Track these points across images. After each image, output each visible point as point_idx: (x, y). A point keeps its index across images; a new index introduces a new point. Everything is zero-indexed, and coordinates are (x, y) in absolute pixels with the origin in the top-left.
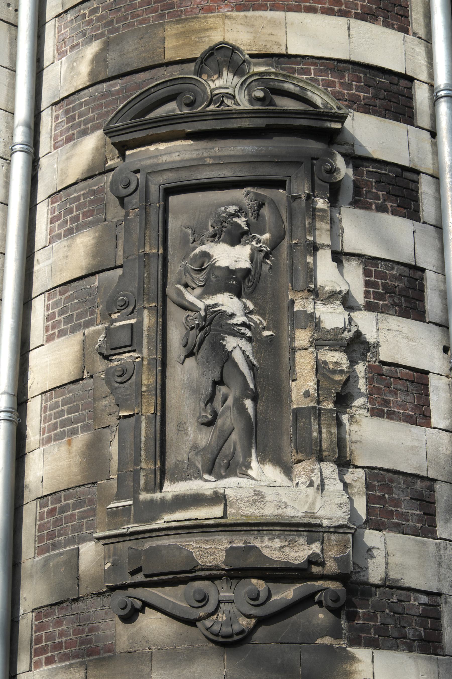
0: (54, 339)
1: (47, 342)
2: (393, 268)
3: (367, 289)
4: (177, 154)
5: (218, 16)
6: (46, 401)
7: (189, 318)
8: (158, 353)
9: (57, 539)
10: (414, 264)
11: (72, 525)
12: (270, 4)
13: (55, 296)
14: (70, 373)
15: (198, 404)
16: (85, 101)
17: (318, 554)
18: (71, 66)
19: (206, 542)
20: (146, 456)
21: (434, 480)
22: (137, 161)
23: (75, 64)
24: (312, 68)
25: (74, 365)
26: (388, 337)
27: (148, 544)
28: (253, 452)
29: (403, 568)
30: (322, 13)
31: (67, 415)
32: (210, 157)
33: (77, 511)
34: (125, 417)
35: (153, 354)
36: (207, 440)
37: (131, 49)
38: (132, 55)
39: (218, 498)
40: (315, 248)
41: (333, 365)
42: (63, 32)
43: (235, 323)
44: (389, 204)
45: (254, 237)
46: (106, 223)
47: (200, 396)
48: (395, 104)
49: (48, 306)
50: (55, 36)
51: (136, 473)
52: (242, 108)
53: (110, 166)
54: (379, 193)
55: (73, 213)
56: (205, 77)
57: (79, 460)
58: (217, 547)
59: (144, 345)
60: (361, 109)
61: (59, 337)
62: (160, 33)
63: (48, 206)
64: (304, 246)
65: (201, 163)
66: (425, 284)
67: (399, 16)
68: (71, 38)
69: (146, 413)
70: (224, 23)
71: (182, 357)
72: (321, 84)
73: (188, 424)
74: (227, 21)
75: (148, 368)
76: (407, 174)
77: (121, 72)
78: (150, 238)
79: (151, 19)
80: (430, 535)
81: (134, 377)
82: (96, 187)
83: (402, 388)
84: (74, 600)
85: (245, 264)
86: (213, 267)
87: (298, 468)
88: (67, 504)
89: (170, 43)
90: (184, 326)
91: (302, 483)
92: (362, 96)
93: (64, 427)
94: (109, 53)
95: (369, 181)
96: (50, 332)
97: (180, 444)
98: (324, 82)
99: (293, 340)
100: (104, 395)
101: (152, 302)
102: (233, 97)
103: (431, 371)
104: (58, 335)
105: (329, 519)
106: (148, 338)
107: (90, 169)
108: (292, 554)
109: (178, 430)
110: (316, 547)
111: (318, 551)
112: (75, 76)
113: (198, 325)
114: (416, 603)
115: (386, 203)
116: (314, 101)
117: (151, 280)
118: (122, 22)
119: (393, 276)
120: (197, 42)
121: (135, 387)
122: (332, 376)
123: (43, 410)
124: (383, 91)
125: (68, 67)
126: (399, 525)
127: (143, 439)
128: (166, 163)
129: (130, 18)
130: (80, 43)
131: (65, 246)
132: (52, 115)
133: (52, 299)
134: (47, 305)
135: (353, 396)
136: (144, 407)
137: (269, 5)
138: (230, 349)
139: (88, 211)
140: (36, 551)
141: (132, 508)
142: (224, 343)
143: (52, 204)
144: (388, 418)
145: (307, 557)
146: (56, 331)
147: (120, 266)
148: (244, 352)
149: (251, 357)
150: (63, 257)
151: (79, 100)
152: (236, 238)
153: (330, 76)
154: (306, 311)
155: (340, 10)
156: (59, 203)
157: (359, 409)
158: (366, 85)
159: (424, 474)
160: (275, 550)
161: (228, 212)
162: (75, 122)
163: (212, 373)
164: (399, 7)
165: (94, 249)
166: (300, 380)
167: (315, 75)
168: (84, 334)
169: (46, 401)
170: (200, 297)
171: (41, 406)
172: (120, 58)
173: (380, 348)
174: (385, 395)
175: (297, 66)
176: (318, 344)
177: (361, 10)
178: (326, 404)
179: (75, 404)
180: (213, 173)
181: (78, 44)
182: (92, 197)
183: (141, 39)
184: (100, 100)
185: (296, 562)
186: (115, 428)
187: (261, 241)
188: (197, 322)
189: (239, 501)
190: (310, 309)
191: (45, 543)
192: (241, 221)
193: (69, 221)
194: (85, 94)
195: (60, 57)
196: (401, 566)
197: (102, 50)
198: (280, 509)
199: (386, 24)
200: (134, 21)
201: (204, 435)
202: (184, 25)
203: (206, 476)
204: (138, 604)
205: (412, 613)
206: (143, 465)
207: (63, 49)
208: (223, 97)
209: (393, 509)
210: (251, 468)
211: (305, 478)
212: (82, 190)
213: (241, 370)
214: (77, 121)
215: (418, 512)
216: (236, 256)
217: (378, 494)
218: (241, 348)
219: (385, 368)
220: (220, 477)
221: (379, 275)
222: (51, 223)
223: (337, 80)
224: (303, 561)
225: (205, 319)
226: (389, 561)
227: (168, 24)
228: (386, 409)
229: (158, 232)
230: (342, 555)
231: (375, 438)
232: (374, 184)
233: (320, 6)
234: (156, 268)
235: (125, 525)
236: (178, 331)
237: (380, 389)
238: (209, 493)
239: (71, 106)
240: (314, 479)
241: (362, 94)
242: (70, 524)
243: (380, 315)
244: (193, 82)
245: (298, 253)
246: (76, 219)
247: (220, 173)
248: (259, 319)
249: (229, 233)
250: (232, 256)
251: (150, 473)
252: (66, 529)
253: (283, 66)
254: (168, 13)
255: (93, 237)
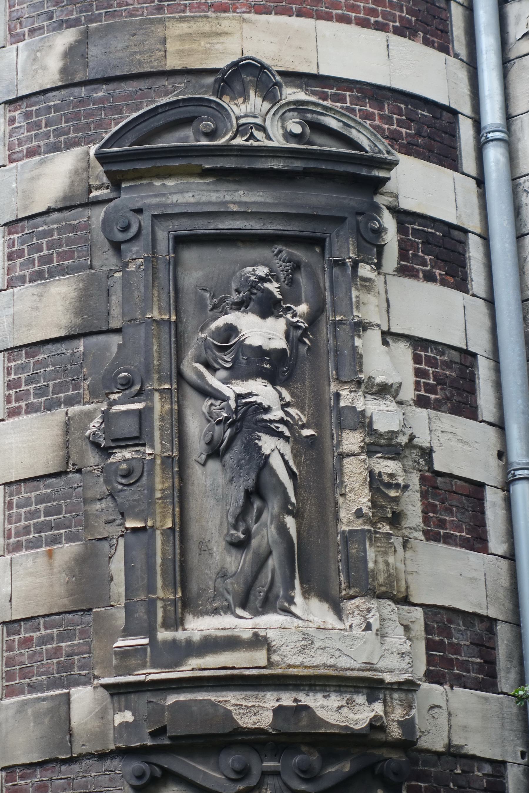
0: (19, 414)
1: (8, 416)
2: (443, 354)
3: (418, 379)
4: (191, 194)
5: (234, 19)
6: (11, 495)
7: (213, 408)
8: (174, 450)
9: (35, 678)
10: (465, 347)
11: (57, 663)
12: (296, 8)
13: (19, 357)
14: (48, 463)
15: (225, 517)
16: (55, 105)
17: (381, 717)
18: (33, 56)
19: (247, 698)
20: (164, 581)
21: (495, 620)
22: (137, 197)
23: (39, 54)
24: (348, 94)
25: (52, 453)
26: (442, 440)
27: (171, 699)
28: (297, 582)
29: (466, 731)
30: (357, 24)
31: (45, 516)
32: (234, 203)
33: (64, 644)
34: (135, 530)
35: (168, 451)
36: (237, 565)
37: (120, 46)
38: (122, 54)
39: (258, 641)
40: (361, 327)
41: (388, 477)
42: (17, 8)
43: (272, 419)
44: (437, 272)
45: (289, 309)
46: (93, 271)
47: (228, 508)
48: (439, 144)
49: (9, 369)
50: (5, 11)
51: (151, 604)
52: (275, 144)
53: (96, 196)
54: (426, 257)
55: (42, 251)
56: (226, 98)
57: (65, 579)
58: (261, 705)
59: (155, 438)
60: (404, 150)
61: (27, 412)
62: (159, 30)
63: (4, 237)
64: (350, 324)
65: (222, 210)
66: (476, 372)
67: (439, 32)
68: (29, 19)
69: (162, 526)
70: (241, 28)
71: (204, 457)
72: (358, 115)
73: (213, 543)
74: (244, 25)
75: (162, 469)
76: (456, 234)
77: (107, 75)
78: (159, 301)
79: (145, 11)
80: (491, 689)
81: (144, 479)
82: (75, 222)
83: (458, 504)
84: (64, 762)
85: (280, 343)
86: (241, 344)
87: (349, 605)
88: (48, 635)
89: (172, 46)
90: (205, 417)
91: (357, 625)
92: (404, 133)
93: (40, 532)
94: (89, 47)
95: (415, 241)
96: (14, 404)
97: (203, 568)
98: (361, 113)
99: (339, 443)
100: (98, 497)
101: (165, 383)
102: (262, 128)
103: (487, 483)
104: (25, 410)
105: (391, 672)
106: (160, 429)
107: (65, 199)
108: (352, 716)
109: (201, 550)
110: (378, 708)
111: (381, 713)
112: (40, 71)
113: (227, 418)
114: (480, 774)
115: (434, 270)
116: (359, 141)
117: (162, 354)
118: (104, 9)
119: (444, 363)
120: (209, 49)
121: (146, 491)
122: (386, 491)
123: (6, 506)
124: (426, 127)
125: (28, 57)
126: (459, 677)
127: (159, 561)
128: (176, 205)
129: (115, 5)
130: (44, 27)
131: (33, 294)
132: (5, 116)
133: (14, 360)
134: (8, 368)
135: (406, 515)
136: (158, 519)
137: (294, 9)
138: (267, 452)
139: (65, 252)
140: (4, 691)
141: (149, 649)
142: (260, 444)
143: (9, 234)
144: (445, 543)
145: (368, 720)
146: (23, 404)
147: (118, 331)
148: (282, 456)
149: (291, 463)
150: (31, 308)
151: (45, 103)
152: (268, 308)
153: (368, 105)
154: (354, 408)
155: (376, 22)
156: (20, 235)
157: (413, 531)
158: (408, 119)
159: (484, 612)
160: (331, 710)
161: (257, 276)
162: (40, 131)
163: (244, 481)
164: (438, 20)
165: (78, 304)
166: (350, 495)
167: (351, 103)
168: (67, 413)
169: (11, 495)
170: (226, 381)
171: (5, 500)
172: (104, 57)
173: (434, 455)
174: (441, 514)
175: (330, 91)
176: (370, 450)
177: (399, 23)
178: (381, 526)
179: (55, 503)
180: (238, 223)
181: (41, 28)
182: (71, 235)
183: (133, 35)
184: (77, 107)
185: (357, 727)
186: (115, 541)
187: (296, 314)
188: (225, 415)
189: (284, 646)
190: (361, 405)
191: (18, 681)
192: (273, 287)
193: (36, 261)
194: (54, 96)
195: (13, 40)
196: (465, 728)
197: (79, 42)
198: (334, 659)
199: (427, 42)
200: (122, 10)
201: (233, 558)
202: (190, 25)
203: (239, 611)
204: (158, 772)
205: (476, 786)
206: (160, 593)
207: (19, 30)
208: (251, 128)
209: (453, 657)
210: (295, 604)
211: (360, 619)
212: (55, 223)
213: (281, 479)
214: (44, 129)
215: (479, 660)
216: (269, 331)
217: (437, 638)
218: (279, 451)
219: (439, 479)
220: (256, 613)
221: (431, 362)
222: (9, 260)
223: (376, 112)
224: (365, 725)
225: (236, 412)
226: (452, 722)
227: (169, 21)
228: (442, 531)
229: (169, 293)
230: (407, 717)
231: (454, 578)
232: (420, 246)
233: (354, 15)
234: (168, 339)
235: (139, 670)
236: (196, 422)
237: (435, 506)
238: (247, 635)
239: (34, 108)
240: (371, 621)
241: (404, 130)
242: (55, 661)
243: (433, 413)
244: (213, 105)
245: (344, 331)
246: (47, 260)
247: (246, 224)
248: (297, 414)
249: (260, 302)
250: (263, 332)
251: (169, 605)
252: (49, 666)
253: (313, 89)
254: (168, 5)
255: (75, 287)
